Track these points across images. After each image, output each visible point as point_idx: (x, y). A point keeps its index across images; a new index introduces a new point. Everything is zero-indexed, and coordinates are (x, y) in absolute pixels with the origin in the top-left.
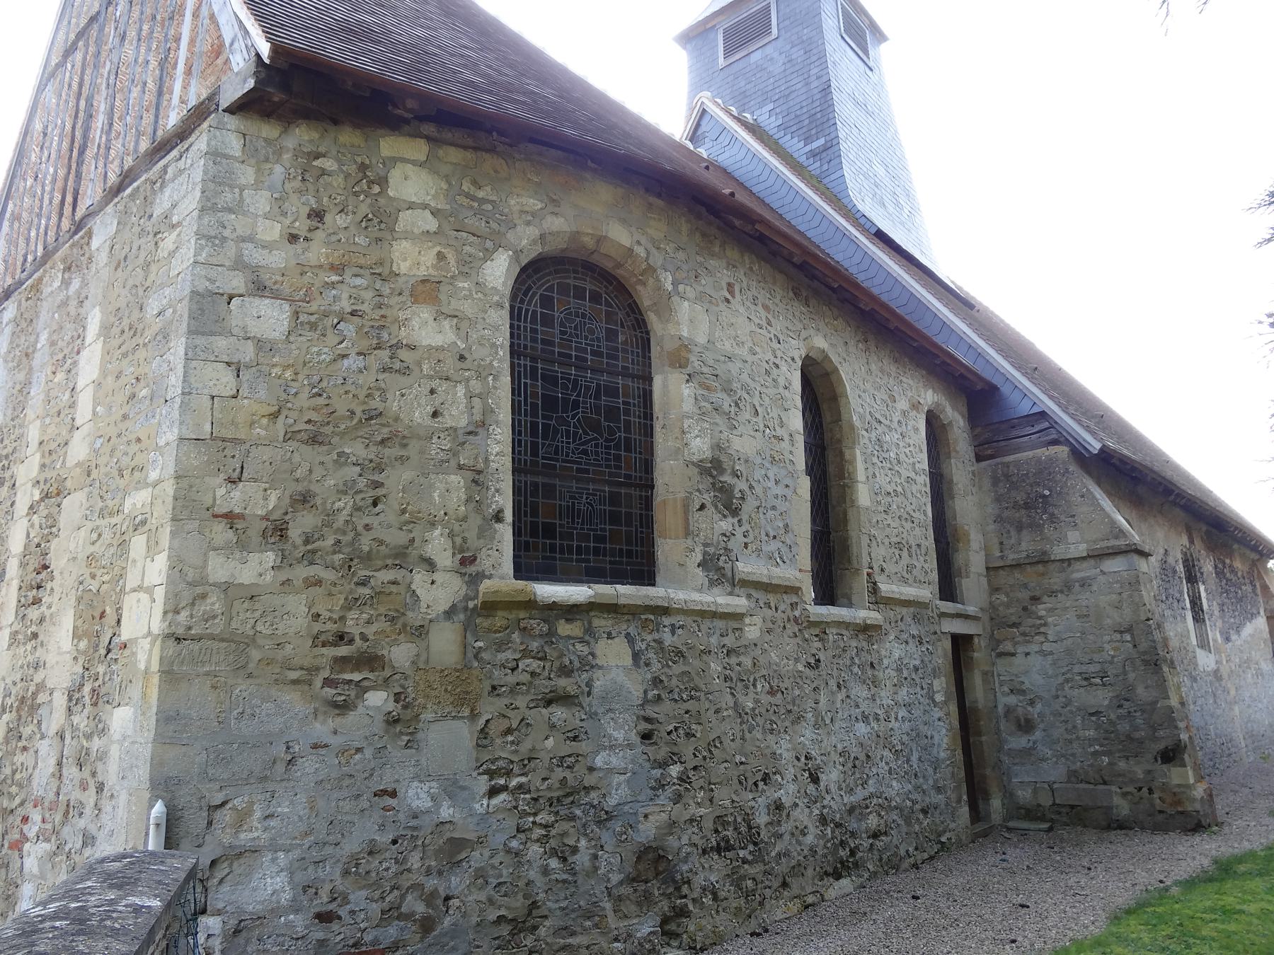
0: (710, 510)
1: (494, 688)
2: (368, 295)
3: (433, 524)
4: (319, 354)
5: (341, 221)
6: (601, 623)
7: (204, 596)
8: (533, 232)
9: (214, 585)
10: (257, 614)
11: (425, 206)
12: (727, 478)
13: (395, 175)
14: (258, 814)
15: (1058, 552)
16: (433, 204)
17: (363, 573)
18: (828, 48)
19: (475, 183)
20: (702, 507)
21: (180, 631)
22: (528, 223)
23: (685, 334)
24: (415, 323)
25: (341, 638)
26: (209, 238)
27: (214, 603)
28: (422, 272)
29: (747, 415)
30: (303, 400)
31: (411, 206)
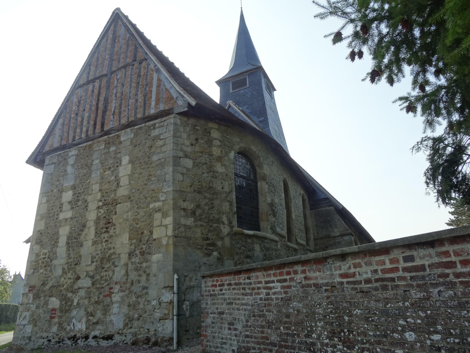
0: (271, 216)
1: (237, 253)
2: (208, 159)
3: (223, 214)
4: (199, 172)
5: (202, 141)
6: (255, 240)
7: (180, 227)
8: (238, 147)
9: (182, 225)
10: (191, 232)
11: (218, 139)
12: (274, 208)
13: (212, 131)
14: (194, 279)
15: (332, 234)
16: (219, 139)
17: (211, 224)
18: (264, 93)
19: (227, 134)
20: (270, 215)
21: (176, 235)
22: (237, 145)
23: (265, 173)
24: (217, 166)
25: (208, 239)
26: (175, 143)
27: (182, 229)
28: (218, 155)
29: (276, 193)
30: (196, 183)
31: (215, 139)
